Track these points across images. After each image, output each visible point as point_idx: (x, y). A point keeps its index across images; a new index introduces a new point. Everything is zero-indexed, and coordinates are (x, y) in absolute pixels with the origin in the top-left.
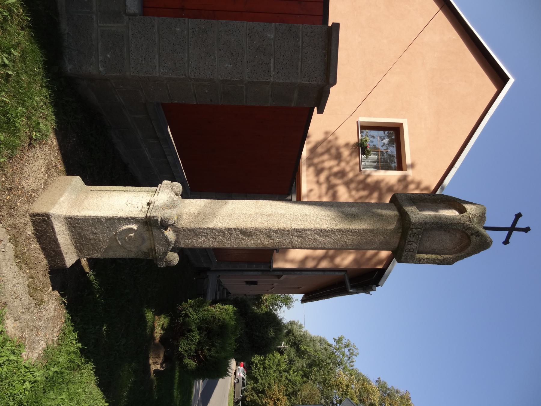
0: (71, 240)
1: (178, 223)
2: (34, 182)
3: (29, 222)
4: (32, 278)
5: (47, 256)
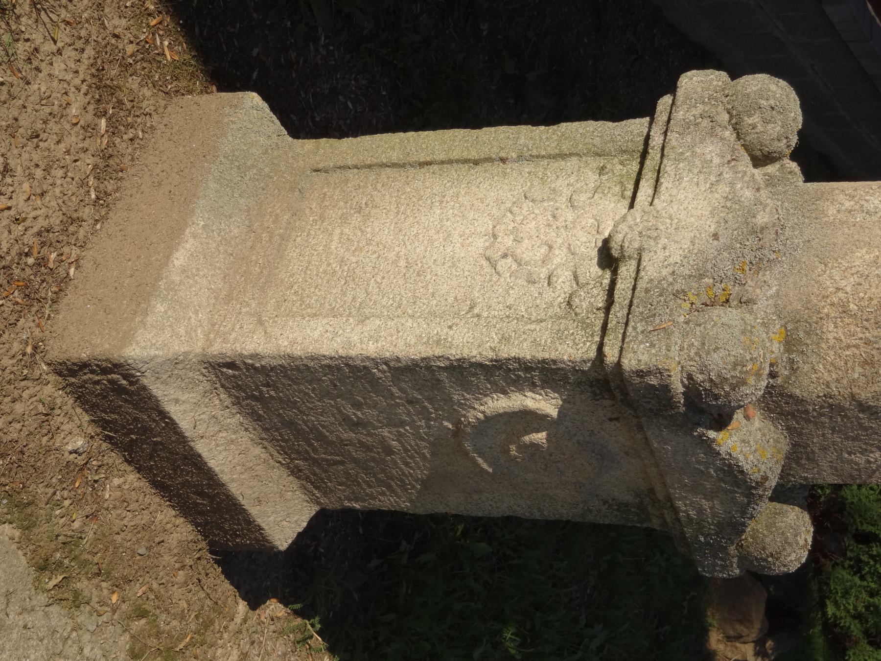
0: (265, 448)
1: (794, 370)
2: (42, 195)
3: (58, 401)
4: (142, 614)
5: (186, 510)
